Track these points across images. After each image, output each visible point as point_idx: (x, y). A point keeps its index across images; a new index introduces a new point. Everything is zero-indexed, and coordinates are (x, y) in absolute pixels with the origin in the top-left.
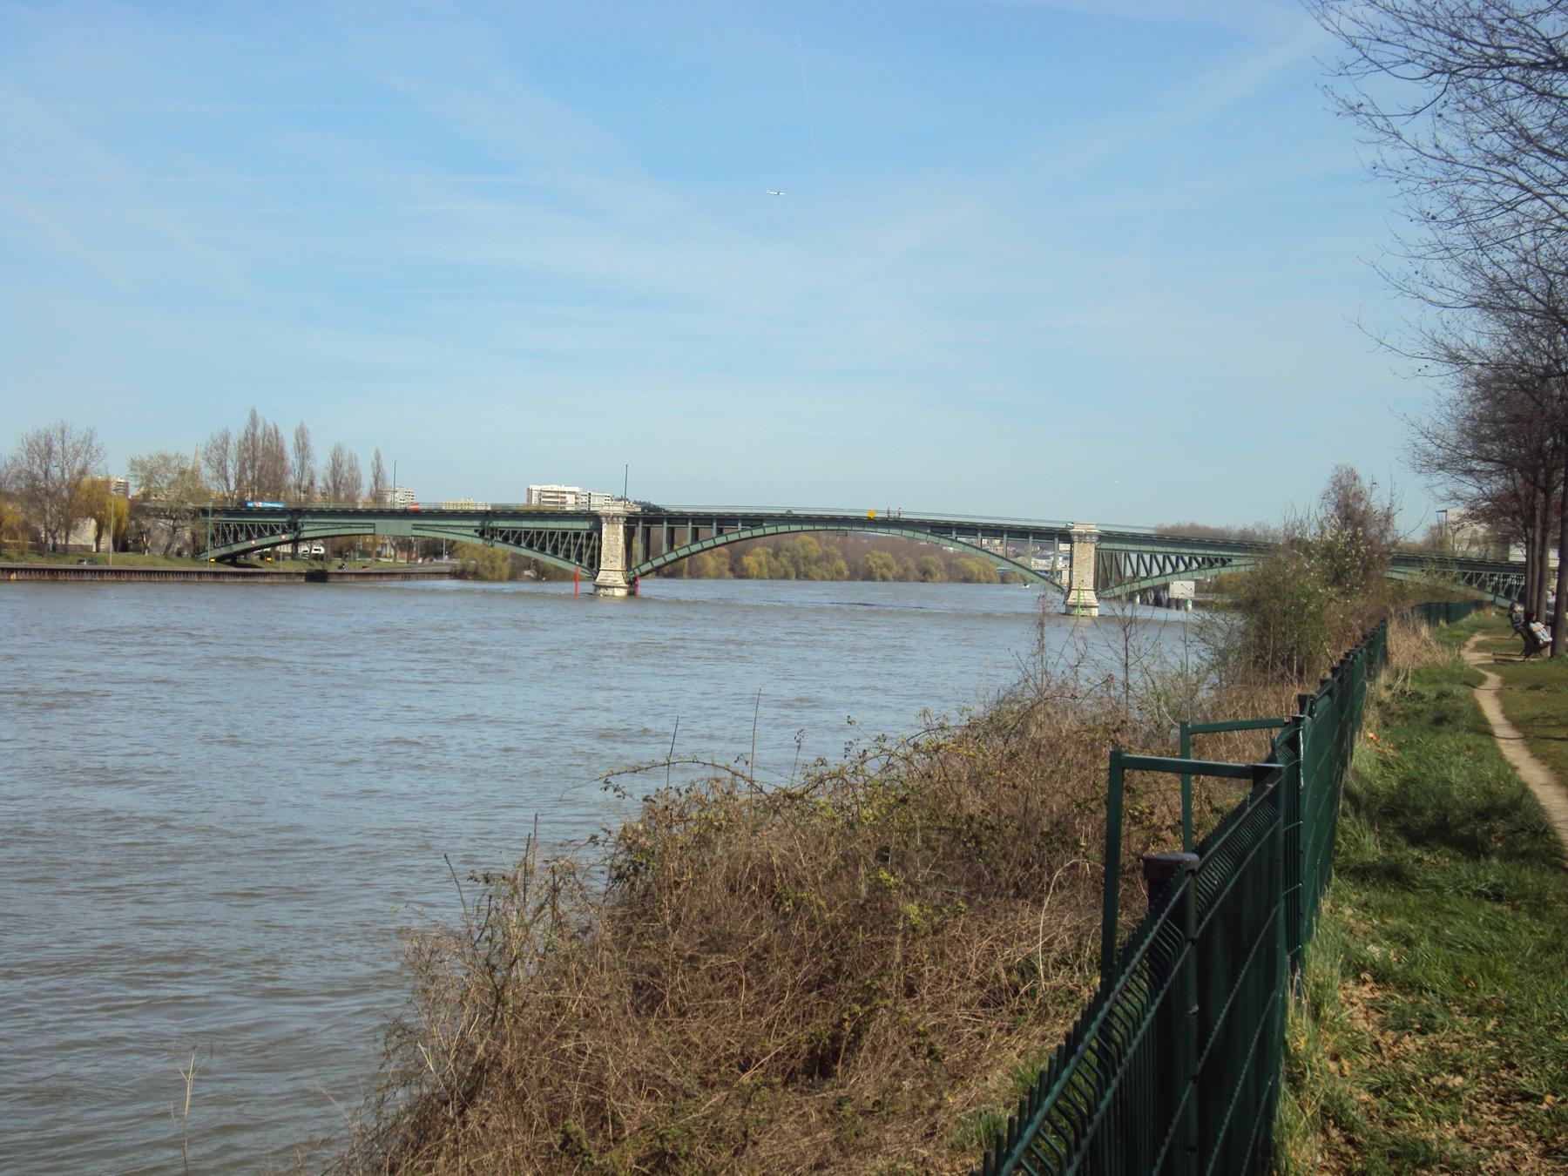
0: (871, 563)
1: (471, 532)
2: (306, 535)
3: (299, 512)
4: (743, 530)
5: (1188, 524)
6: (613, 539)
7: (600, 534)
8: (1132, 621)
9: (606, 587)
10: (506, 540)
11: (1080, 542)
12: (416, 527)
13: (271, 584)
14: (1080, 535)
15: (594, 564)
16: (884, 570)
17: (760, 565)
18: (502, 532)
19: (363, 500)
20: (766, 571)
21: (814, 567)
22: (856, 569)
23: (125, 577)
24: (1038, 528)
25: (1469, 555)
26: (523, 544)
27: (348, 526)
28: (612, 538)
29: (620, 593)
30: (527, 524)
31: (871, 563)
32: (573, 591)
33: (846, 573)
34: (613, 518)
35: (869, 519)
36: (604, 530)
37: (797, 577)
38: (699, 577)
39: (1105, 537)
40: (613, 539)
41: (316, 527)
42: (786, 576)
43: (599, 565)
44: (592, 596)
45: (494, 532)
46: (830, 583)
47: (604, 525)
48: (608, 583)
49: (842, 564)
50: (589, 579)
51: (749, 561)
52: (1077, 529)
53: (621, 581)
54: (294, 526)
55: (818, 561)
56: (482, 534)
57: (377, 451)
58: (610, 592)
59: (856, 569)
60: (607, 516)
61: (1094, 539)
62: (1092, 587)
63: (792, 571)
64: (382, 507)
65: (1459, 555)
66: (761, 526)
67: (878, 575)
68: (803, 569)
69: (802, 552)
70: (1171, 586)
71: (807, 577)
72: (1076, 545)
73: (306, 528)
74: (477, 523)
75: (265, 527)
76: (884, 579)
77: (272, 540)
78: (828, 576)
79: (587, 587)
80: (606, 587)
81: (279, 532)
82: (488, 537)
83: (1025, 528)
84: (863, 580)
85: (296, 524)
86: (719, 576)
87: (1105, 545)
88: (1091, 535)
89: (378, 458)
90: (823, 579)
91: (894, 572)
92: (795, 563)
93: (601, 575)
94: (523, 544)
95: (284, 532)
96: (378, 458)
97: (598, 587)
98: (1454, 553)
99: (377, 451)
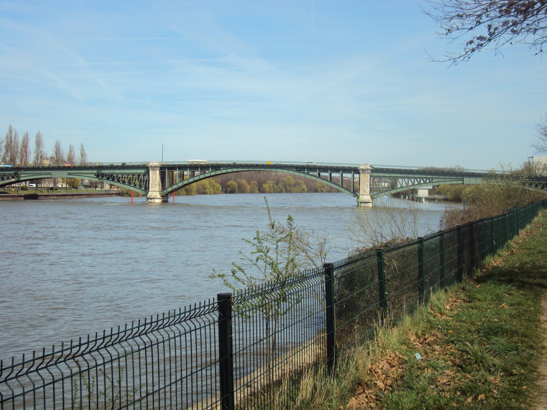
0: (317, 186)
1: (93, 176)
2: (22, 179)
3: (19, 169)
4: (212, 171)
5: (449, 167)
6: (155, 177)
7: (149, 175)
8: (418, 210)
9: (151, 199)
10: (108, 179)
11: (363, 173)
12: (69, 174)
13: (54, 199)
14: (363, 170)
15: (147, 189)
16: (322, 188)
17: (270, 187)
18: (106, 175)
19: (77, 161)
20: (272, 189)
21: (292, 188)
22: (311, 188)
23: (105, 195)
24: (344, 167)
25: (543, 175)
26: (116, 180)
27: (40, 174)
28: (154, 176)
29: (158, 201)
30: (117, 171)
31: (317, 186)
32: (131, 201)
33: (306, 190)
34: (154, 168)
35: (268, 165)
36: (150, 173)
37: (286, 192)
38: (244, 193)
39: (375, 170)
40: (155, 177)
41: (26, 175)
42: (281, 192)
43: (149, 189)
44: (143, 204)
45: (103, 175)
46: (301, 194)
47: (151, 171)
48: (152, 197)
49: (304, 187)
50: (144, 195)
51: (265, 186)
52: (361, 167)
53: (158, 195)
54: (16, 175)
55: (294, 186)
56: (98, 176)
57: (82, 144)
58: (153, 201)
59: (311, 188)
60: (151, 167)
61: (369, 171)
62: (369, 193)
63: (284, 190)
64: (73, 165)
65: (538, 175)
66: (220, 169)
67: (319, 190)
68: (288, 189)
69: (288, 182)
70: (418, 192)
71: (290, 192)
72: (361, 174)
73: (22, 176)
74: (95, 171)
75: (5, 175)
76: (322, 192)
77: (8, 181)
78: (298, 191)
79: (144, 199)
80: (151, 199)
81: (10, 178)
82: (101, 177)
83: (338, 167)
84: (313, 192)
85: (17, 174)
86: (252, 192)
87: (375, 174)
88: (368, 170)
89: (82, 146)
90: (297, 192)
91: (326, 189)
92: (285, 186)
93: (150, 193)
94: (116, 180)
95: (13, 177)
96: (82, 146)
97: (148, 199)
98: (536, 174)
99: (82, 144)
